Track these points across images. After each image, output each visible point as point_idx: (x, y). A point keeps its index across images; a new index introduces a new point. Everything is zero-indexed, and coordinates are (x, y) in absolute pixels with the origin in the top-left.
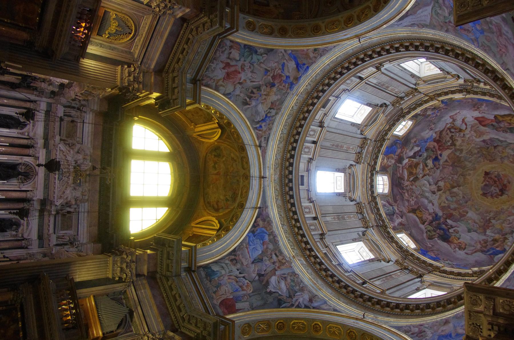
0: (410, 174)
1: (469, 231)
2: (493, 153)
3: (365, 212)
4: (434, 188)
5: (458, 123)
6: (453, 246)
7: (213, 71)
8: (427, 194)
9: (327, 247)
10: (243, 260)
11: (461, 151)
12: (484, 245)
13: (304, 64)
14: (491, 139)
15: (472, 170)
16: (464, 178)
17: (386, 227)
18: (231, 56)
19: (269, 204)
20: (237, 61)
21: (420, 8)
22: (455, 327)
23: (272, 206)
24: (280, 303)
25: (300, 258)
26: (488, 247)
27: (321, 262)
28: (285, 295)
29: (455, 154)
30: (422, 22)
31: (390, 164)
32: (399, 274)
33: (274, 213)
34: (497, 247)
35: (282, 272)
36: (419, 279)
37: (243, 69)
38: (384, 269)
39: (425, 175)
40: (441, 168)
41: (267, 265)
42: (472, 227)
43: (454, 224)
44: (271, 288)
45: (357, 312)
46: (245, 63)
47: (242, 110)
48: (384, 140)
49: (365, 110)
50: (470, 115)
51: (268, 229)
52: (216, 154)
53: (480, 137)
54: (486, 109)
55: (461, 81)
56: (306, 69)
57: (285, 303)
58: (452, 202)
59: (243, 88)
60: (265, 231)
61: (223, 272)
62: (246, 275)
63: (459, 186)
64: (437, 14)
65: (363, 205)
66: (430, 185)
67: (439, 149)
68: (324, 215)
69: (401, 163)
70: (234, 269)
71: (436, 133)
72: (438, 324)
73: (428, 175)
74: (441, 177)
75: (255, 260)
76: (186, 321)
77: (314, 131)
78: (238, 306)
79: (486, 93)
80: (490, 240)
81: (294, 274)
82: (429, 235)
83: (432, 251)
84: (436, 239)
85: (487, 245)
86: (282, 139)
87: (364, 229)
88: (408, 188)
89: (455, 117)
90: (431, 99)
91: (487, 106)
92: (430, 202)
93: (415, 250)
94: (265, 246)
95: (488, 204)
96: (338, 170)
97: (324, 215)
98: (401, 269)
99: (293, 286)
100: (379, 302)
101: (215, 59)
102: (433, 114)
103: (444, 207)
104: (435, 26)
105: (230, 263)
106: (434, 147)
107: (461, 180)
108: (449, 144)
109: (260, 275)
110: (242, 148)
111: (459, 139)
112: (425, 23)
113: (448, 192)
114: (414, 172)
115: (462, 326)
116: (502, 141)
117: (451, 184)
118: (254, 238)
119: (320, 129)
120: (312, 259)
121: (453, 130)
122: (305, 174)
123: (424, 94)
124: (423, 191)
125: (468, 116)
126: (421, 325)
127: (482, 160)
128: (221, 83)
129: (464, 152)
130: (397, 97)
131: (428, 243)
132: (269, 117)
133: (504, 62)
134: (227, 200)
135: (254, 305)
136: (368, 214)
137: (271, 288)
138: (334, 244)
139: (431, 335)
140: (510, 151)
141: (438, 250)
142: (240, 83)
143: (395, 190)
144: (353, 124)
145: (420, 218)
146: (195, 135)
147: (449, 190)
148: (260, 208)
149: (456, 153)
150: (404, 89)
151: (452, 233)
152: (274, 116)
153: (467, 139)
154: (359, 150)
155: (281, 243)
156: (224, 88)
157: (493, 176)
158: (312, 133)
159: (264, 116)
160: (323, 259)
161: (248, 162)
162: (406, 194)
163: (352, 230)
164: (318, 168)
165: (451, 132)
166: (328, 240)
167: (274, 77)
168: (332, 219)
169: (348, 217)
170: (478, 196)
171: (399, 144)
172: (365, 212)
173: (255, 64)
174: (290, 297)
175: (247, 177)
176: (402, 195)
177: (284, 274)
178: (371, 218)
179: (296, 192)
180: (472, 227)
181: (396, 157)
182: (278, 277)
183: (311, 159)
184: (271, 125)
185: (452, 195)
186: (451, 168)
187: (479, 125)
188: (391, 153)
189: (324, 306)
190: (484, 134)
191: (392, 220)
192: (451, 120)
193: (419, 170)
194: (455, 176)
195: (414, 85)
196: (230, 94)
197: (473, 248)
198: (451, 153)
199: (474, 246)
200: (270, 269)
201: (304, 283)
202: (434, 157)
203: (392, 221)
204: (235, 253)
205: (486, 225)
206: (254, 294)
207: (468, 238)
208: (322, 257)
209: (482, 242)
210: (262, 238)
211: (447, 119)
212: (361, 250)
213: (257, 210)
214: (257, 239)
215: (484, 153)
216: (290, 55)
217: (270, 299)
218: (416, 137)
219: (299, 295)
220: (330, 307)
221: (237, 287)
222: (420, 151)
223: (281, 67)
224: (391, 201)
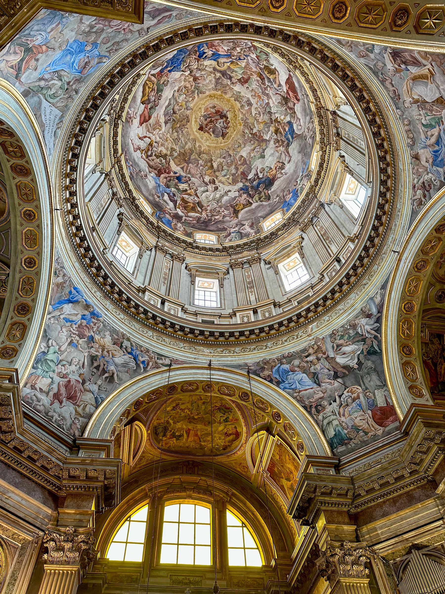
0: (193, 209)
1: (263, 157)
2: (180, 116)
3: (241, 260)
4: (211, 187)
5: (143, 145)
7: (64, 419)
8: (218, 196)
9: (290, 301)
10: (317, 396)
11: (173, 150)
12: (280, 144)
13: (70, 292)
14: (165, 115)
15: (195, 143)
17: (259, 239)
18: (45, 389)
19: (241, 362)
20: (52, 382)
21: (41, 115)
22: (425, 147)
24: (374, 352)
25: (310, 329)
26: (284, 139)
27: (314, 304)
29: (176, 158)
30: (57, 121)
34: (285, 130)
36: (326, 206)
37: (64, 376)
39: (196, 195)
41: (322, 367)
42: (259, 153)
43: (253, 172)
44: (353, 363)
46: (56, 371)
47: (120, 385)
48: (158, 227)
49: (123, 240)
51: (273, 364)
52: (162, 434)
53: (160, 126)
56: (77, 292)
57: (372, 346)
58: (228, 170)
59: (90, 380)
60: (276, 368)
61: (335, 423)
62: (336, 394)
63: (212, 160)
64: (54, 96)
66: (207, 191)
67: (169, 173)
69: (182, 217)
70: (329, 409)
73: (196, 191)
74: (200, 178)
75: (315, 382)
76: (417, 468)
78: (381, 403)
80: (275, 137)
81: (333, 335)
82: (264, 199)
83: (284, 197)
84: (269, 192)
85: (281, 140)
86: (160, 338)
87: (262, 263)
88: (209, 214)
89: (135, 147)
90: (119, 161)
92: (226, 193)
94: (296, 369)
95: (235, 133)
98: (313, 225)
99: (350, 337)
101: (47, 414)
103: (233, 179)
104: (66, 106)
105: (321, 414)
106: (166, 178)
109: (336, 376)
110: (171, 388)
112: (58, 118)
113: (217, 173)
114: (192, 205)
116: (169, 104)
118: (287, 382)
119: (147, 293)
120: (310, 315)
121: (149, 153)
123: (111, 169)
125: (136, 132)
126: (414, 187)
127: (186, 129)
128: (80, 410)
129: (174, 147)
130: (112, 199)
131: (275, 200)
132: (132, 350)
133: (138, 31)
135: (379, 383)
136: (244, 257)
137: (353, 363)
138: (284, 294)
139: (430, 175)
140: (181, 98)
141: (283, 191)
142: (84, 382)
143: (212, 228)
145: (245, 206)
146: (132, 464)
147: (215, 172)
148: (248, 372)
149: (175, 156)
150: (106, 185)
151: (263, 175)
152: (131, 343)
156: (88, 406)
157: (205, 123)
159: (130, 356)
160: (310, 302)
161: (190, 383)
162: (216, 217)
163: (264, 274)
164: (192, 304)
165: (151, 156)
167: (81, 336)
168: (252, 295)
169: (248, 278)
170: (225, 142)
171: (160, 214)
172: (241, 260)
173: (60, 358)
174: (364, 340)
175: (208, 386)
176: (217, 222)
177: (333, 347)
178: (249, 253)
179: (227, 329)
180: (259, 153)
181: (175, 221)
182: (337, 354)
184: (142, 349)
185: (220, 169)
186: (190, 165)
189: (378, 300)
190: (159, 121)
192: (138, 151)
193: (190, 199)
195: (101, 175)
196: (96, 399)
199: (281, 154)
201: (346, 324)
204: (308, 407)
205: (258, 139)
206: (362, 383)
208: (308, 303)
209: (277, 144)
210: (286, 372)
211: (137, 155)
212: (287, 268)
213: (251, 375)
214: (287, 379)
215: (178, 125)
216: (54, 309)
219: (361, 329)
220: (379, 294)
221: (354, 405)
223: (68, 324)
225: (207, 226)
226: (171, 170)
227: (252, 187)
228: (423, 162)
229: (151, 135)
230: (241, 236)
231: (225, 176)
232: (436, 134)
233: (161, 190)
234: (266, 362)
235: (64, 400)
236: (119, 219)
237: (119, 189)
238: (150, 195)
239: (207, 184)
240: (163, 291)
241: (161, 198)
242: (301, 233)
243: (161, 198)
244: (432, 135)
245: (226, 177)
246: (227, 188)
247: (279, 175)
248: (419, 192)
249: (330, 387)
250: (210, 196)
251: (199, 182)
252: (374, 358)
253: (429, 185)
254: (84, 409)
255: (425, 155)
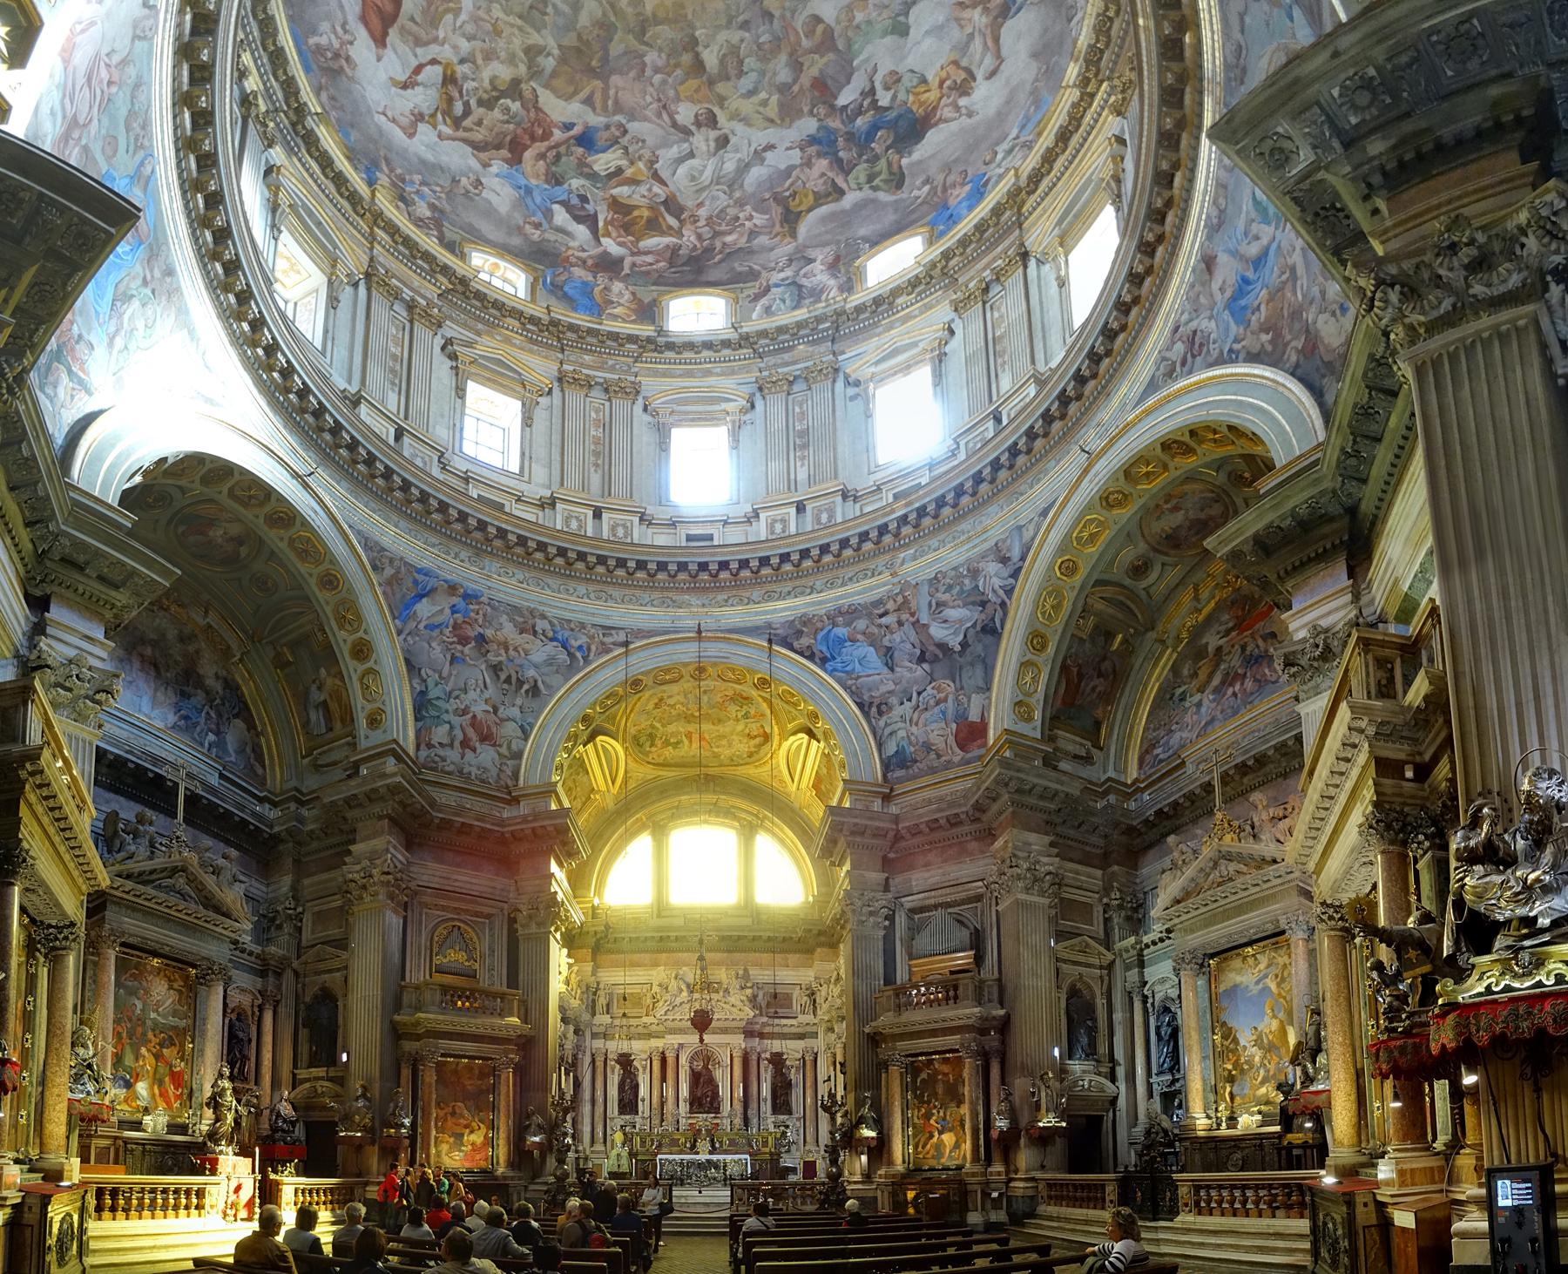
0: (654, 226)
1: (902, 30)
3: (786, 370)
4: (702, 140)
5: (423, 98)
6: (947, 112)
7: (486, 770)
8: (730, 167)
10: (883, 689)
11: (533, 52)
13: (416, 582)
16: (657, 21)
17: (839, 313)
19: (760, 620)
20: (452, 728)
22: (1234, 254)
23: (766, 613)
24: (991, 631)
27: (918, 509)
28: (976, 615)
29: (554, 74)
31: (627, 296)
32: (996, 315)
33: (782, 609)
35: (925, 608)
36: (1032, 264)
37: (465, 712)
38: (970, 350)
39: (656, 176)
40: (619, 118)
41: (903, 640)
44: (955, 642)
45: (1072, 461)
47: (551, 696)
48: (555, 323)
50: (377, 72)
51: (819, 625)
54: (325, 26)
55: (277, 155)
57: (993, 619)
61: (902, 733)
63: (692, 44)
65: (765, 373)
66: (691, 155)
67: (547, 135)
68: (792, 485)
69: (621, 260)
70: (898, 711)
71: (486, 165)
72: (1198, 288)
73: (651, 163)
74: (659, 115)
77: (567, 520)
78: (974, 716)
79: (271, 55)
82: (886, 181)
84: (904, 161)
89: (405, 121)
90: (378, 217)
91: (314, 31)
92: (759, 156)
93: (930, 242)
94: (859, 637)
96: (663, 444)
97: (792, 485)
98: (984, 303)
99: (962, 591)
100: (1064, 399)
101: (461, 772)
102: (422, 197)
103: (781, 105)
106: (542, 156)
107: (665, 33)
108: (515, 106)
109: (922, 659)
111: (486, 75)
113: (721, 88)
114: (646, 213)
115: (1246, 234)
117: (688, 76)
119: (559, 506)
121: (458, 108)
122: (683, 532)
123: (371, 249)
124: (717, 180)
125: (382, 76)
126: (1176, 329)
128: (504, 750)
129: (535, 38)
130: (411, 321)
131: (916, 193)
134: (746, 716)
135: (981, 683)
136: (795, 363)
137: (955, 642)
139: (1213, 324)
141: (947, 169)
142: (495, 712)
143: (714, 275)
144: (527, 421)
145: (820, 199)
147: (711, 83)
148: (770, 641)
149: (548, 70)
151: (894, 97)
153: (478, 44)
154: (597, 393)
155: (857, 600)
158: (574, 525)
162: (729, 239)
164: (662, 500)
165: (467, 112)
166: (863, 483)
167: (464, 641)
171: (555, 276)
172: (786, 370)
174: (983, 604)
176: (732, 254)
178: (800, 364)
179: (732, 553)
181: (602, 280)
183: (641, 520)
185: (733, 72)
186: (615, 80)
187: (400, 21)
188: (592, 298)
189: (1027, 535)
191: (817, 293)
192: (422, 127)
194: (647, 59)
196: (522, 727)
197: (977, 44)
198: (554, 91)
199: (971, 36)
200: (913, 637)
202: (580, 150)
203: (822, 291)
207: (928, 44)
210: (841, 642)
211: (425, 143)
213: (775, 647)
216: (405, 622)
217: (978, 648)
218: (520, 229)
221: (936, 710)
222: (565, 204)
223: (437, 632)
224: (752, 288)
225: (700, 271)
226: (552, 124)
227: (850, 137)
228: (1215, 286)
229: (434, 50)
230: (800, 293)
231: (751, 93)
232: (1265, 241)
233: (538, 200)
234: (806, 621)
235: (477, 744)
236: (450, 357)
237: (416, 281)
238: (509, 234)
239: (687, 132)
240: (595, 496)
241: (545, 225)
242: (953, 315)
243: (545, 225)
244: (1257, 238)
245: (755, 99)
246: (760, 137)
247: (947, 112)
248: (1180, 347)
249: (908, 675)
250: (701, 173)
251: (660, 132)
252: (988, 639)
253: (1201, 345)
254: (509, 747)
255: (1227, 271)
